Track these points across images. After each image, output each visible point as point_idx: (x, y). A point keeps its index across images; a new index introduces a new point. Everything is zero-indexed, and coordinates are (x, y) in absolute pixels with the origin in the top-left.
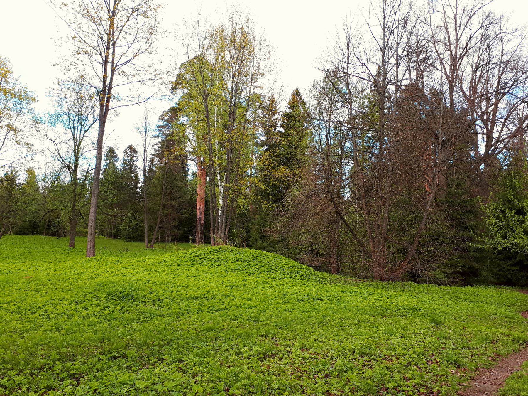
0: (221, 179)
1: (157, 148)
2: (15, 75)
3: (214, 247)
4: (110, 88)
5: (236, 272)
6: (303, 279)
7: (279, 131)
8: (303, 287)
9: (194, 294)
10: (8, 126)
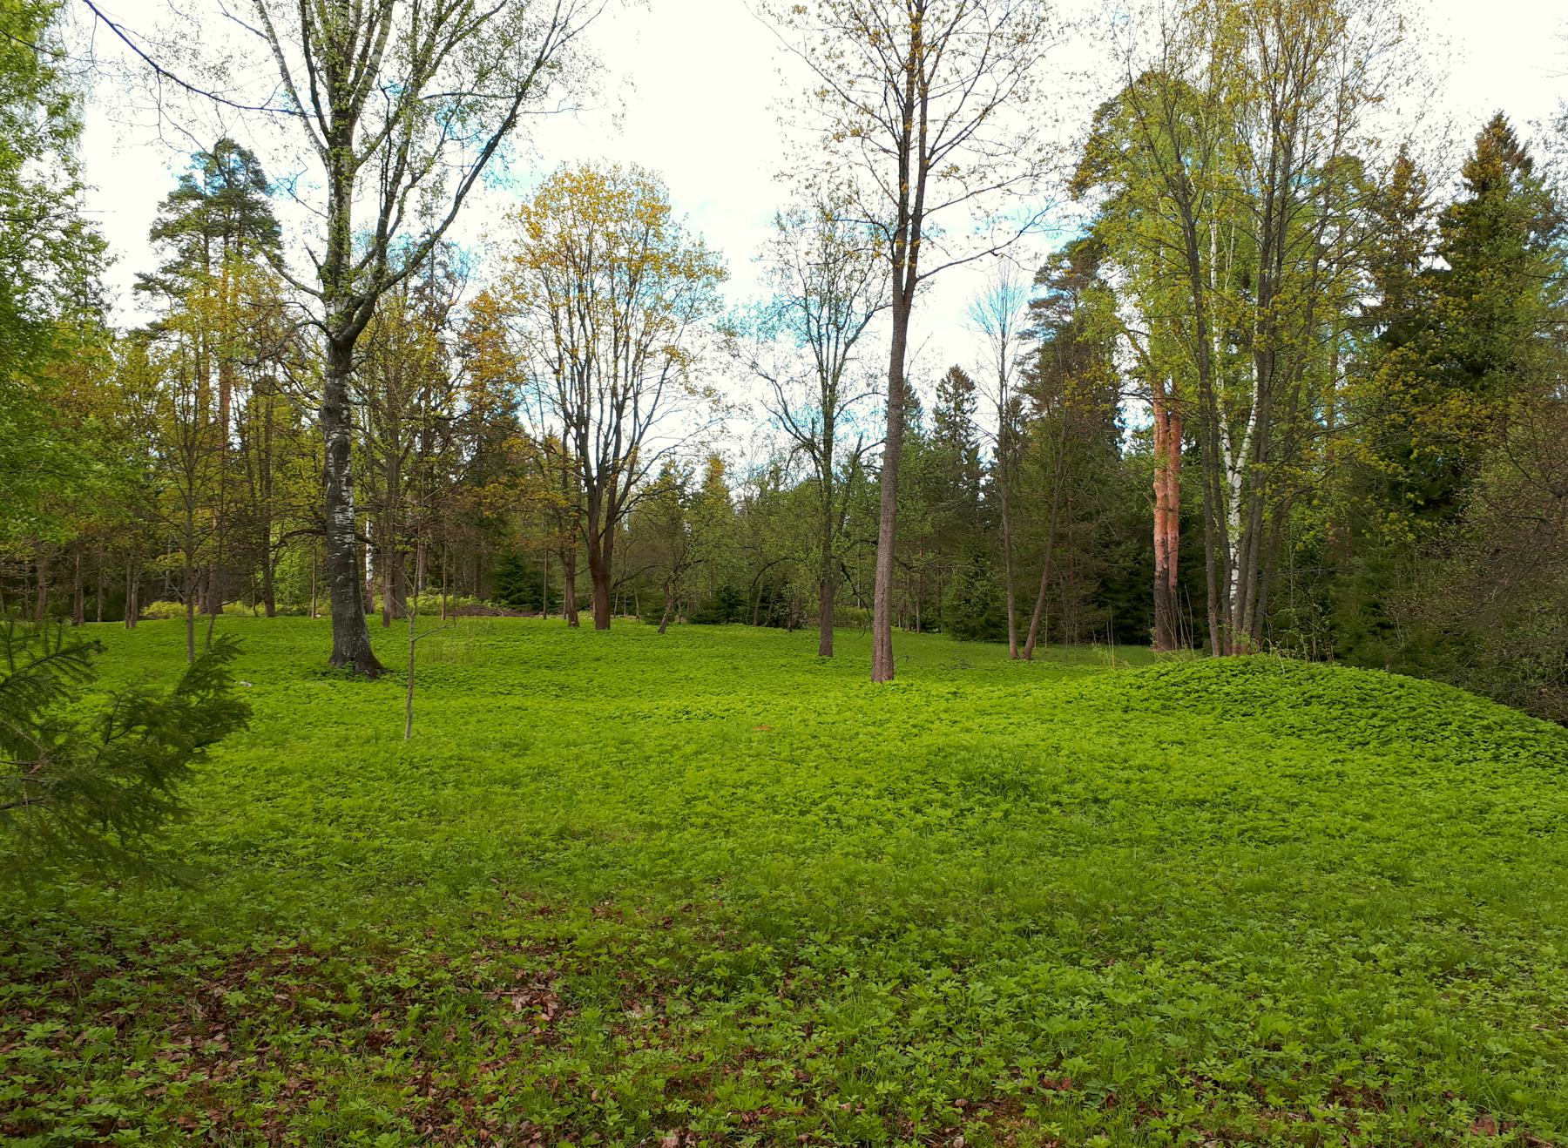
0: (1235, 447)
1: (1028, 367)
2: (675, 215)
3: (1227, 661)
4: (918, 217)
5: (1307, 735)
6: (1544, 767)
7: (1429, 272)
8: (1548, 793)
9: (1194, 793)
10: (666, 350)
